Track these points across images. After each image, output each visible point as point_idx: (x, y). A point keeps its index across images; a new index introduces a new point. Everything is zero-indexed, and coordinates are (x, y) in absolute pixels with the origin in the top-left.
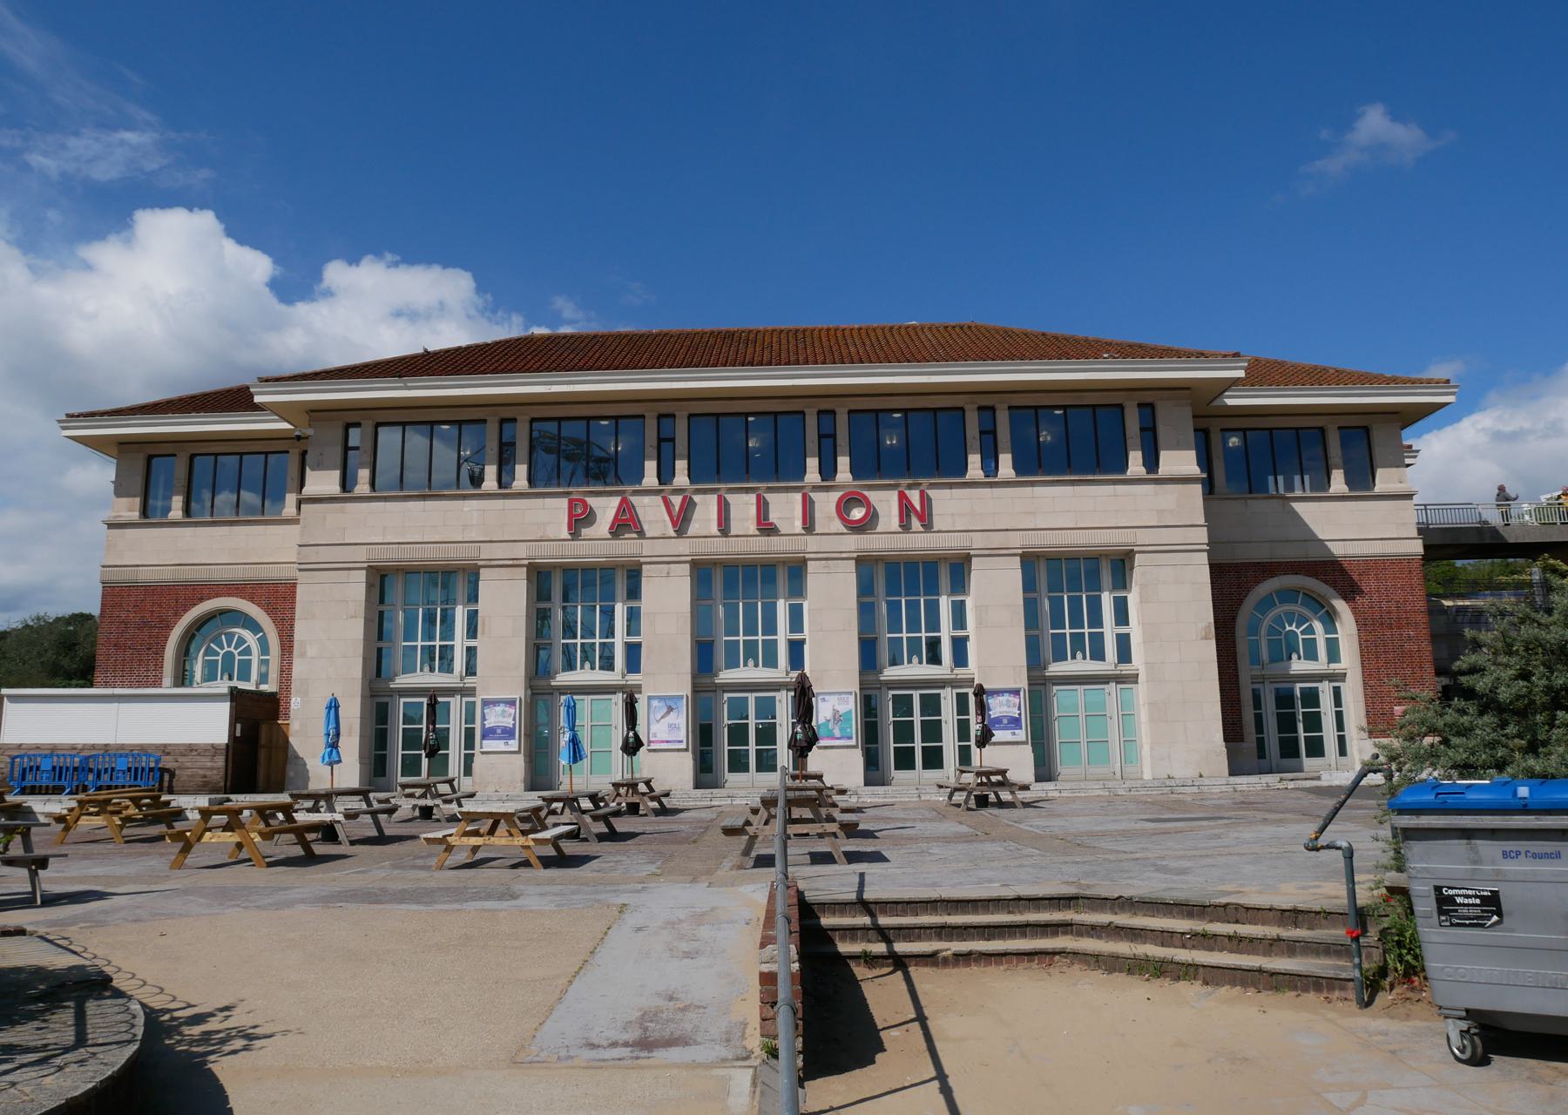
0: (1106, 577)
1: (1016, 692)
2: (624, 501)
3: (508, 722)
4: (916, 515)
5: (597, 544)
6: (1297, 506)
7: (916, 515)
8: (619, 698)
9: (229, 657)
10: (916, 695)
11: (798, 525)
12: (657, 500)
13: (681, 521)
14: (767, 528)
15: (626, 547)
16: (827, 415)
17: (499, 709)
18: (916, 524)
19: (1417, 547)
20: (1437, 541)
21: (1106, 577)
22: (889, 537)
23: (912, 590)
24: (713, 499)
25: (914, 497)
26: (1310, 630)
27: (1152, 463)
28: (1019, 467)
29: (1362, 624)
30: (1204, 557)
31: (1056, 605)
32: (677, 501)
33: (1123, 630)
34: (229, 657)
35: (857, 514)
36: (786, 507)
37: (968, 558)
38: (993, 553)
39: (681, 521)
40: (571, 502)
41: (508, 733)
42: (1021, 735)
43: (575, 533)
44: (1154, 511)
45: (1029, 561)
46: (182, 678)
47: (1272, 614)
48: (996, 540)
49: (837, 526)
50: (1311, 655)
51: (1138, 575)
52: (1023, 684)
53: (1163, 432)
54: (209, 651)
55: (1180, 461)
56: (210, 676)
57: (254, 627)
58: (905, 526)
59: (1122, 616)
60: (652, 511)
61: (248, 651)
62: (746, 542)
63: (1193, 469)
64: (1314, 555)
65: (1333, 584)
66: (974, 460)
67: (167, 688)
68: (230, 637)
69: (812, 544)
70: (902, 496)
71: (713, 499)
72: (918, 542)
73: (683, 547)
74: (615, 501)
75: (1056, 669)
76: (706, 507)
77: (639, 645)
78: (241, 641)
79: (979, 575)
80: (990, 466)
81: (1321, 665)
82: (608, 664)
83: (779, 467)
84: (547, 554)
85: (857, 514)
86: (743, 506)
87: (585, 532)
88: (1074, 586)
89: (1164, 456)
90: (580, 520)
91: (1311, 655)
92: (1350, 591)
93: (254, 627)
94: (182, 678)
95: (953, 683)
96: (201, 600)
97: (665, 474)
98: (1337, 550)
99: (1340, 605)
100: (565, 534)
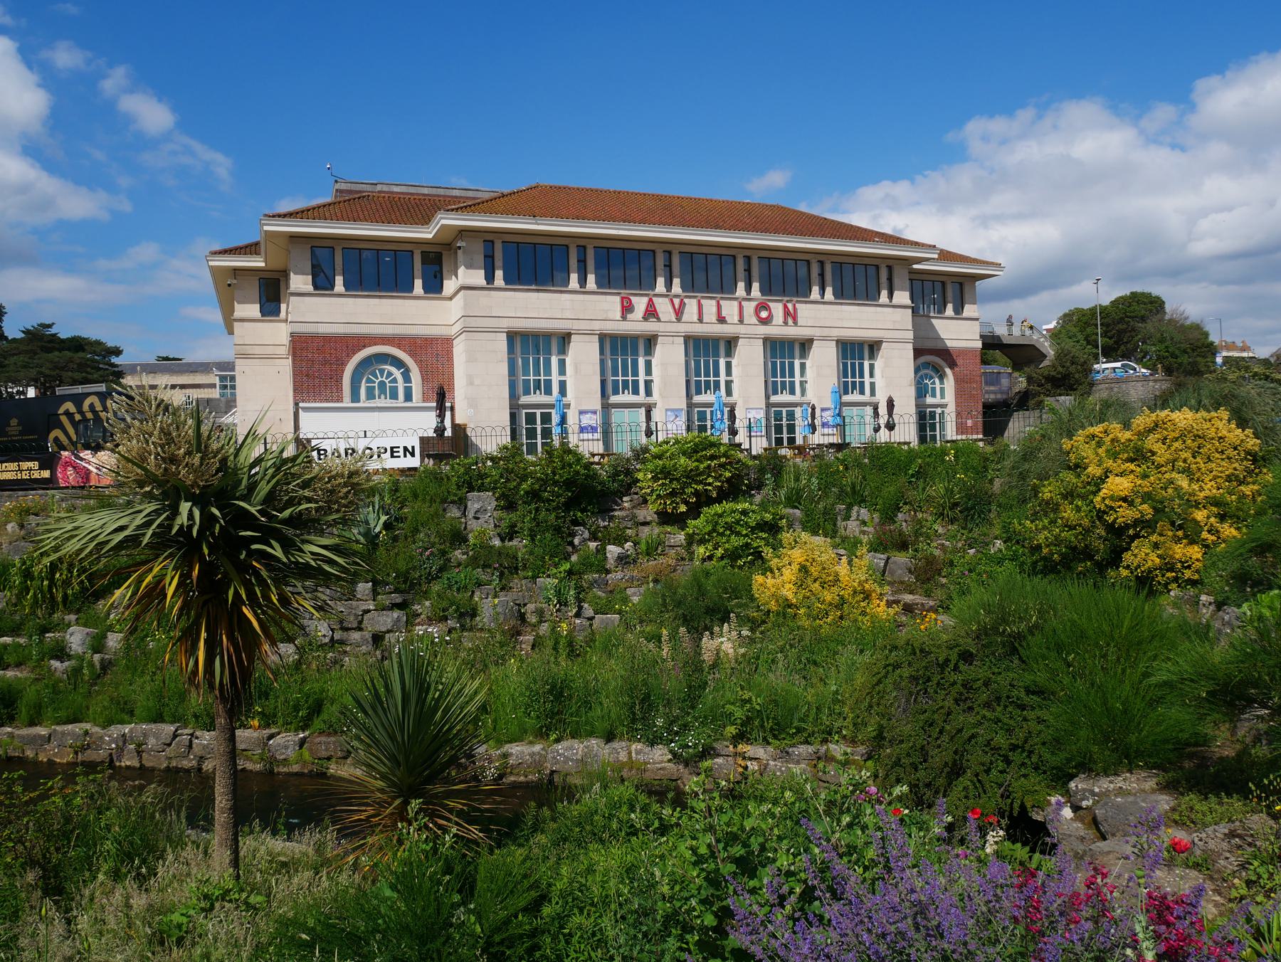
0: (554, 348)
1: (595, 412)
2: (651, 300)
3: (593, 423)
4: (791, 316)
5: (636, 325)
6: (934, 321)
7: (791, 316)
8: (643, 410)
9: (382, 384)
10: (538, 412)
11: (736, 319)
12: (666, 300)
13: (679, 313)
14: (721, 320)
15: (651, 327)
16: (748, 259)
17: (589, 415)
18: (790, 321)
19: (979, 344)
20: (990, 341)
21: (554, 348)
22: (777, 329)
23: (783, 357)
24: (694, 302)
25: (790, 306)
26: (934, 383)
27: (891, 296)
28: (507, 280)
29: (956, 380)
30: (910, 346)
31: (615, 362)
32: (677, 301)
33: (562, 378)
34: (382, 384)
35: (764, 314)
36: (730, 309)
37: (569, 335)
38: (824, 339)
39: (679, 313)
40: (623, 299)
41: (594, 430)
42: (597, 436)
43: (624, 318)
44: (887, 319)
45: (512, 336)
46: (355, 397)
47: (926, 371)
48: (826, 332)
49: (754, 320)
50: (934, 395)
51: (658, 350)
52: (599, 407)
53: (896, 281)
54: (369, 381)
55: (902, 297)
56: (370, 396)
57: (399, 363)
58: (786, 323)
59: (562, 371)
60: (663, 306)
61: (395, 380)
62: (711, 328)
63: (908, 302)
64: (939, 346)
65: (945, 360)
66: (574, 277)
67: (347, 403)
68: (382, 371)
69: (740, 330)
70: (785, 307)
71: (694, 302)
72: (791, 331)
73: (683, 328)
74: (645, 300)
75: (614, 399)
76: (777, 309)
77: (652, 381)
78: (390, 374)
79: (575, 345)
80: (583, 281)
81: (937, 400)
82: (636, 392)
83: (724, 287)
84: (610, 327)
85: (764, 314)
86: (710, 306)
87: (629, 316)
88: (624, 353)
89: (896, 293)
90: (627, 308)
91: (934, 395)
92: (952, 365)
93: (399, 363)
94: (355, 397)
95: (800, 405)
96: (365, 347)
97: (669, 285)
98: (949, 344)
99: (948, 371)
100: (618, 316)
